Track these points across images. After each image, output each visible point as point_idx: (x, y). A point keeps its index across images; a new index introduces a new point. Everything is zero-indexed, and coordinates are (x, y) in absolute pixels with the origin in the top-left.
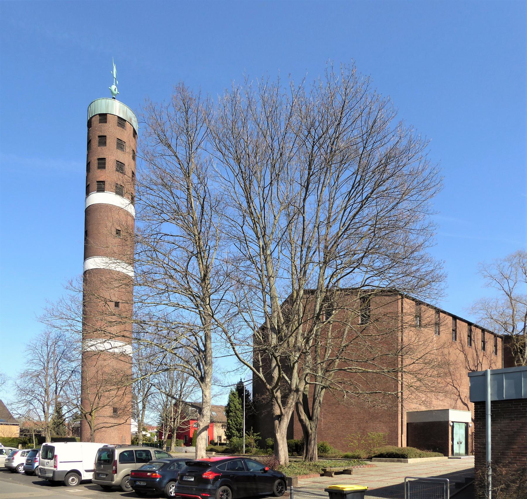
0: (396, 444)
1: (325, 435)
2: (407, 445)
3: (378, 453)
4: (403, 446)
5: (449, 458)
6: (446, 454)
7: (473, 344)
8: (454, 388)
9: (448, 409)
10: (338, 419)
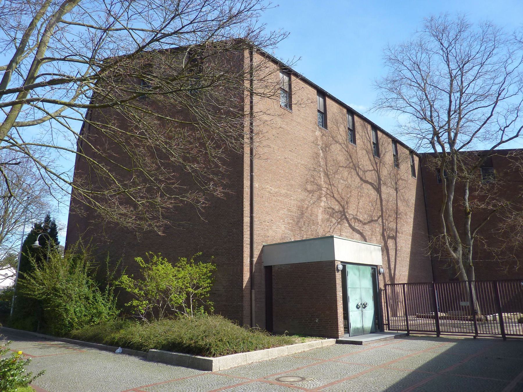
5: (338, 342)
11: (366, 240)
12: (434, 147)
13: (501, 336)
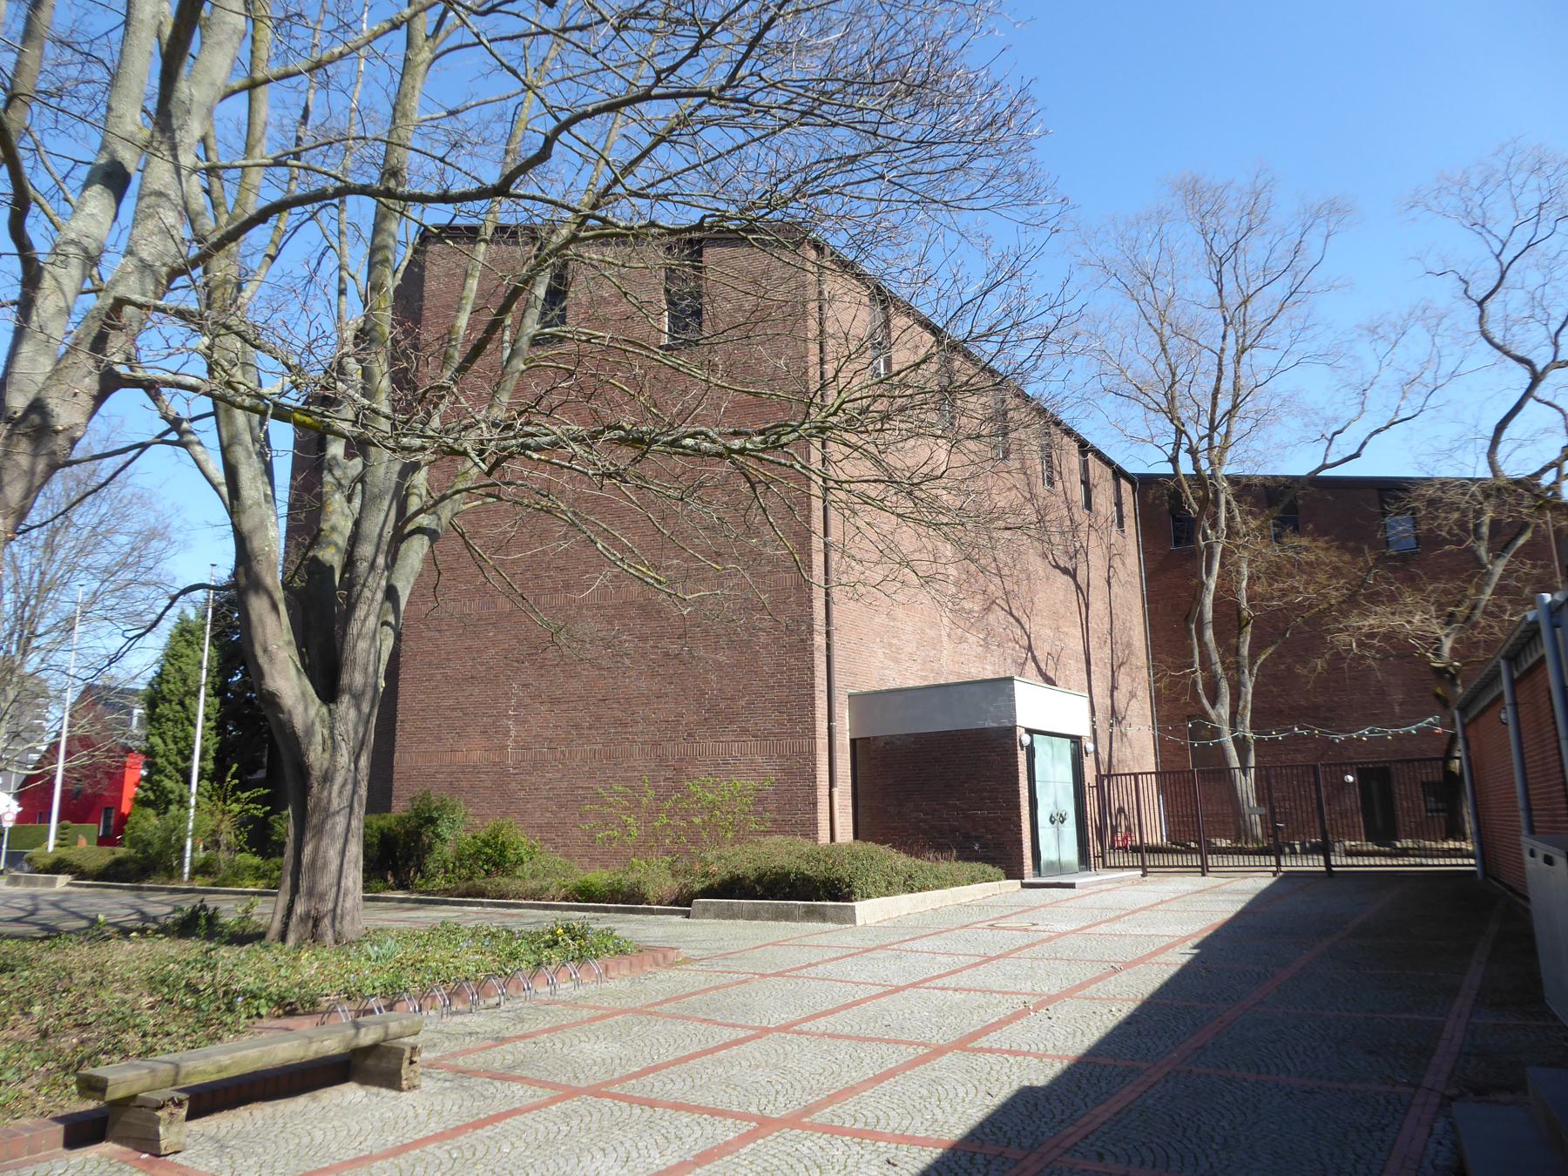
0: (810, 830)
1: (522, 794)
2: (856, 836)
3: (720, 871)
4: (839, 839)
5: (1024, 886)
6: (1014, 872)
7: (1059, 485)
8: (1012, 620)
9: (1011, 679)
10: (577, 726)
11: (1050, 681)
12: (1174, 460)
13: (1324, 869)
